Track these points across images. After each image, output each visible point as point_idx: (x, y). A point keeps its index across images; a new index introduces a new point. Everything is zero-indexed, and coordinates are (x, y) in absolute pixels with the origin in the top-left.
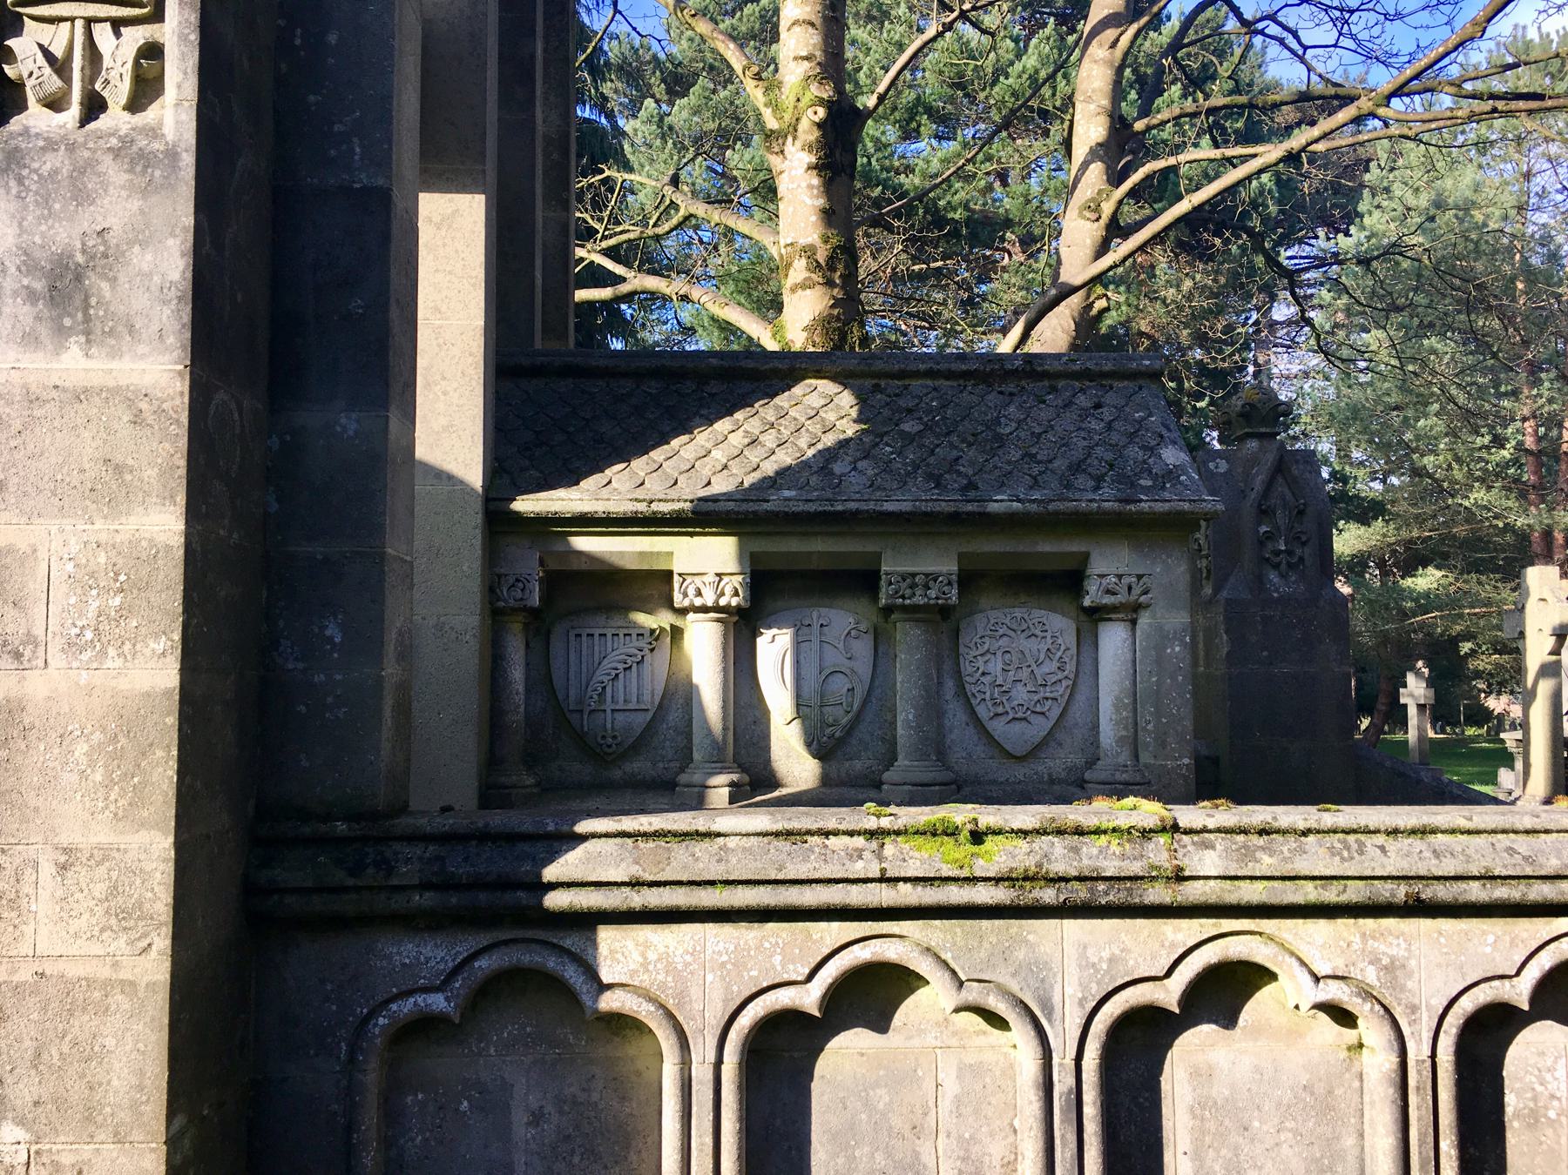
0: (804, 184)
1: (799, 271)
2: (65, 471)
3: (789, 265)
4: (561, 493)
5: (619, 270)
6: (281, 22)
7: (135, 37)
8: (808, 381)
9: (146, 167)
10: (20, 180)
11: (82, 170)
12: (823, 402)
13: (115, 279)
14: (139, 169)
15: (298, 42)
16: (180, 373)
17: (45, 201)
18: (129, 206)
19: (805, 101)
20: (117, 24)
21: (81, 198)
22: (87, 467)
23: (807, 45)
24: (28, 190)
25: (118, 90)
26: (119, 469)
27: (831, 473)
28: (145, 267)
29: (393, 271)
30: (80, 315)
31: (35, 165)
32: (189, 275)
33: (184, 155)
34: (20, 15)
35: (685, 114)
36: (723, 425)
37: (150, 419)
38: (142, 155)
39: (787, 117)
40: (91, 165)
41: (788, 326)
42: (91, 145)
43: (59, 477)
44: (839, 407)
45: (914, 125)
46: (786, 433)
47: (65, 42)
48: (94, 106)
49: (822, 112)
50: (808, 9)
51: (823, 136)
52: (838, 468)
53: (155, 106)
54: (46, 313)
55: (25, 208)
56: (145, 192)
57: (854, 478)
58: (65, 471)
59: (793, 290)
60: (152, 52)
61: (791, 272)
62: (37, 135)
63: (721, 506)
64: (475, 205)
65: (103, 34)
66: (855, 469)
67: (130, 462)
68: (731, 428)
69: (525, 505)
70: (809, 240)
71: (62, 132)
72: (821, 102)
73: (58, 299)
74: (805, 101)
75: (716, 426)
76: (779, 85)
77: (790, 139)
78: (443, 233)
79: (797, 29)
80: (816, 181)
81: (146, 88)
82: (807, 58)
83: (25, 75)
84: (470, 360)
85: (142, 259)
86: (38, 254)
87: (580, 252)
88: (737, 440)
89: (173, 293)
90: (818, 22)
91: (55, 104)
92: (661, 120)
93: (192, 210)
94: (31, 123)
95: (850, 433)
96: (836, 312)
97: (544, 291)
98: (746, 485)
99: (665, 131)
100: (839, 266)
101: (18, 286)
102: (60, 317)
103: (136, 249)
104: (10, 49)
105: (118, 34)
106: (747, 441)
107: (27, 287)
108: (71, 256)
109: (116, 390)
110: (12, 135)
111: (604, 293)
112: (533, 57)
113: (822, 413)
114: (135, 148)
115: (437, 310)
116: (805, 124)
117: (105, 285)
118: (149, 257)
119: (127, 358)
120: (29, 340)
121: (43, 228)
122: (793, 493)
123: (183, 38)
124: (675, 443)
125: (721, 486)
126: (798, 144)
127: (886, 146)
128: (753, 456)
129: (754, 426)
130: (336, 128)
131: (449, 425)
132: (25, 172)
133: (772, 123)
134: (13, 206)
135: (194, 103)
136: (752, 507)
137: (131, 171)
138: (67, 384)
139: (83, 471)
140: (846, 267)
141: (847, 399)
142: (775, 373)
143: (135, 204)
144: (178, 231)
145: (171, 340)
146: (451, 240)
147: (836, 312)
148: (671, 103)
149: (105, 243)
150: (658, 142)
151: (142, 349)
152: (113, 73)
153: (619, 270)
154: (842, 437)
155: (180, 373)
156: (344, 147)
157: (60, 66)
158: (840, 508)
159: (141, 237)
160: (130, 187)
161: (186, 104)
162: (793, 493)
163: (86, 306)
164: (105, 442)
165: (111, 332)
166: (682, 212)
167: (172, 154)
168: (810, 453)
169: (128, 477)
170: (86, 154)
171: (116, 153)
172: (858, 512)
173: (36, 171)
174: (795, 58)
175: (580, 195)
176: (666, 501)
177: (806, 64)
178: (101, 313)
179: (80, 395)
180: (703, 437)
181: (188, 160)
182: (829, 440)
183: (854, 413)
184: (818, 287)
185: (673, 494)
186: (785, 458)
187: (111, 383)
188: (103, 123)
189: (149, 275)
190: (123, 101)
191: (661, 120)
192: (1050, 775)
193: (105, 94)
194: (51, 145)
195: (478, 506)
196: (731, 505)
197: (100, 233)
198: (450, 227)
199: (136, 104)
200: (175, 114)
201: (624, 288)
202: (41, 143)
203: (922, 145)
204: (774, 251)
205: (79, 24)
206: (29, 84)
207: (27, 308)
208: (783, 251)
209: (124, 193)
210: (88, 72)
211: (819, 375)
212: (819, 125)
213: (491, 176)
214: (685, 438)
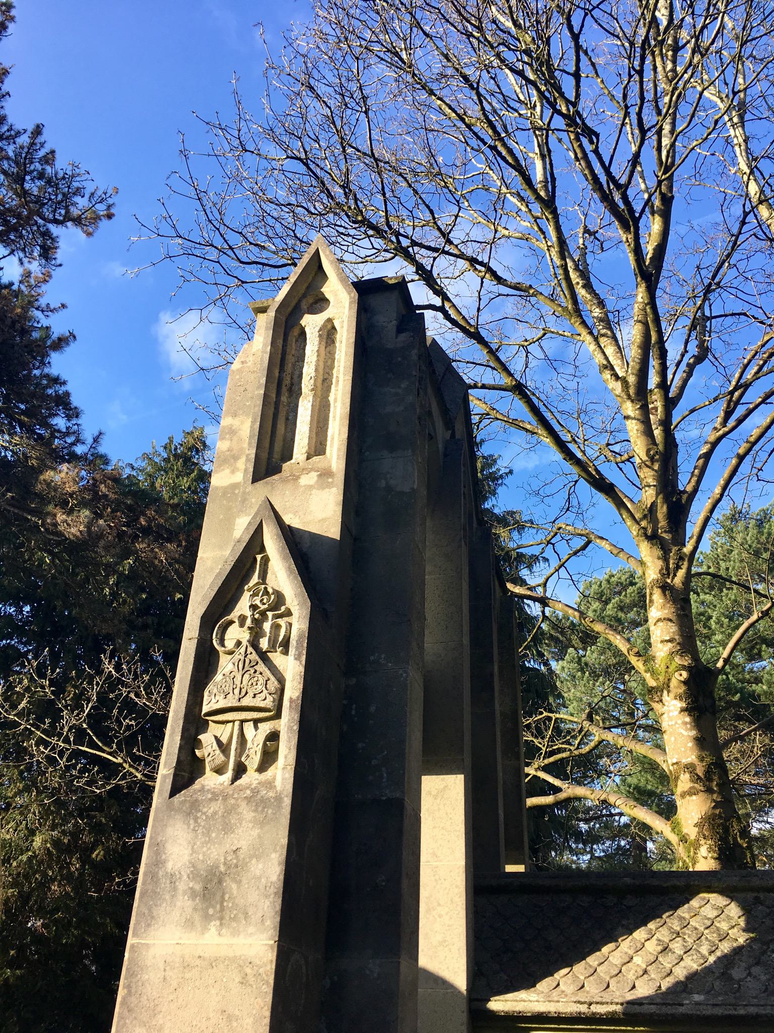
0: (680, 722)
1: (684, 782)
2: (198, 1019)
3: (677, 778)
4: (522, 994)
5: (557, 782)
6: (345, 702)
7: (265, 728)
8: (701, 895)
9: (264, 808)
10: (196, 819)
11: (230, 811)
12: (715, 913)
13: (240, 881)
14: (260, 809)
15: (353, 712)
16: (271, 946)
17: (208, 833)
18: (252, 833)
19: (672, 668)
20: (256, 722)
21: (228, 829)
22: (211, 1015)
23: (669, 633)
24: (199, 826)
25: (253, 760)
26: (230, 1018)
27: (730, 978)
28: (258, 873)
29: (404, 853)
30: (218, 906)
31: (205, 810)
32: (282, 877)
33: (286, 799)
34: (208, 721)
35: (595, 655)
36: (640, 934)
37: (251, 979)
38: (263, 800)
39: (661, 678)
40: (235, 807)
41: (683, 822)
42: (236, 796)
43: (194, 1023)
44: (729, 918)
45: (756, 651)
46: (690, 941)
47: (228, 734)
48: (241, 769)
49: (685, 674)
50: (666, 611)
51: (689, 689)
52: (737, 973)
53: (272, 768)
54: (200, 906)
55: (196, 837)
56: (262, 824)
57: (750, 983)
58: (198, 1019)
59: (683, 796)
60: (274, 737)
61: (679, 783)
62: (208, 790)
63: (646, 1009)
64: (458, 782)
65: (249, 729)
66: (749, 974)
67: (237, 1013)
68: (646, 936)
69: (498, 1004)
70: (689, 760)
71: (221, 788)
72: (684, 668)
73: (208, 896)
74: (672, 668)
75: (634, 934)
76: (653, 658)
77: (665, 692)
78: (438, 801)
79: (660, 624)
80: (688, 719)
81: (269, 757)
82: (669, 641)
83: (206, 755)
84: (456, 890)
85: (256, 867)
86: (200, 866)
87: (527, 770)
88: (652, 947)
89: (272, 890)
90: (674, 619)
91: (219, 771)
92: (579, 659)
93: (287, 834)
94: (206, 783)
95: (741, 941)
96: (717, 811)
97: (506, 825)
98: (663, 988)
99: (583, 666)
100: (715, 777)
101: (186, 887)
102: (207, 908)
103: (254, 861)
104: (200, 741)
105: (256, 728)
106: (660, 948)
107: (191, 888)
108: (218, 867)
109: (233, 959)
110: (195, 792)
111: (548, 800)
112: (492, 675)
113: (712, 927)
114: (259, 796)
115: (434, 854)
116: (674, 683)
117: (234, 886)
118: (260, 866)
119: (242, 936)
120: (189, 924)
121: (205, 849)
122: (702, 998)
123: (290, 729)
124: (605, 950)
125: (644, 990)
126: (672, 695)
127: (738, 666)
128: (667, 962)
129: (664, 934)
130: (374, 762)
131: (443, 944)
132: (199, 814)
133: (652, 683)
134: (191, 836)
135: (293, 767)
136: (669, 1010)
137: (255, 811)
138: (207, 955)
139: (208, 1019)
140: (720, 778)
141: (734, 910)
142: (676, 889)
143: (256, 832)
144: (278, 848)
145: (268, 923)
146: (442, 807)
147: (717, 811)
148: (585, 649)
149: (237, 858)
150: (579, 674)
151: (251, 929)
152: (252, 751)
153: (557, 782)
154: (735, 945)
155: (271, 946)
156: (377, 774)
157: (224, 748)
158: (742, 1012)
159: (257, 853)
160: (255, 821)
161: (289, 767)
162: (702, 998)
163: (223, 900)
164: (224, 997)
165: (235, 919)
166: (597, 739)
167: (279, 799)
168: (712, 959)
169: (235, 1024)
170: (233, 801)
171: (248, 799)
172: (758, 1016)
173: (205, 813)
174: (662, 642)
175: (528, 726)
176: (602, 1003)
177: (670, 645)
178: (230, 905)
179: (213, 963)
180: (626, 945)
181: (287, 802)
182: (725, 947)
183: (742, 923)
184: (701, 794)
185: (607, 997)
186: (692, 964)
187: (231, 954)
188: (244, 780)
189: (260, 878)
190: (256, 766)
191: (579, 659)
192: (183, 957)
193: (246, 763)
194: (215, 796)
195: (464, 1006)
196: (653, 1009)
197: (235, 852)
198: (442, 797)
199: (262, 768)
200: (282, 773)
201: (562, 796)
202: (210, 796)
203: (764, 663)
204: (664, 766)
205: (237, 723)
206: (207, 761)
207: (190, 902)
208: (671, 768)
209: (250, 825)
210: (239, 751)
211: (710, 890)
212: (685, 683)
213: (468, 761)
214: (611, 946)
